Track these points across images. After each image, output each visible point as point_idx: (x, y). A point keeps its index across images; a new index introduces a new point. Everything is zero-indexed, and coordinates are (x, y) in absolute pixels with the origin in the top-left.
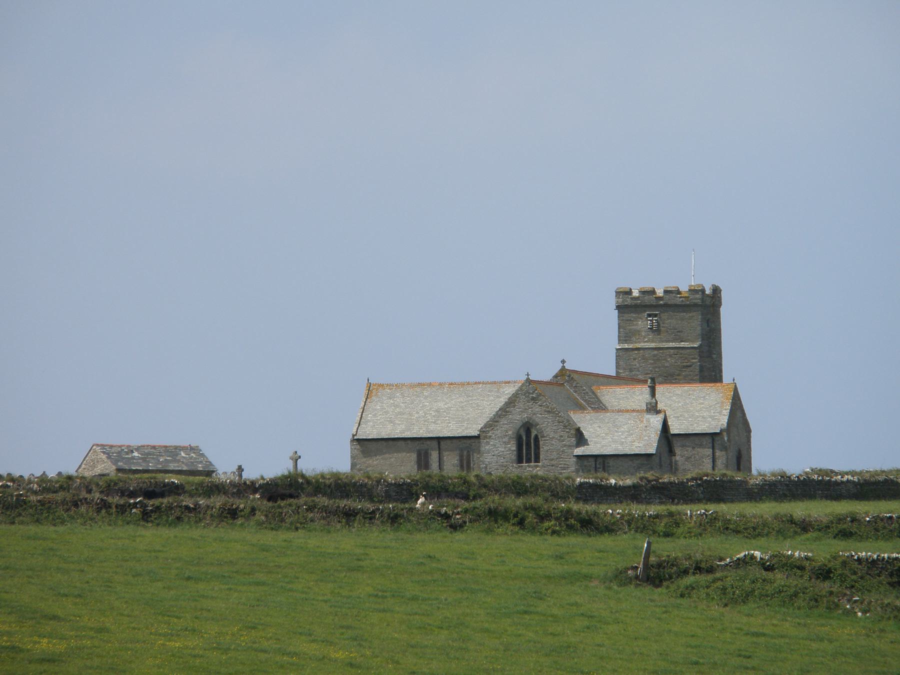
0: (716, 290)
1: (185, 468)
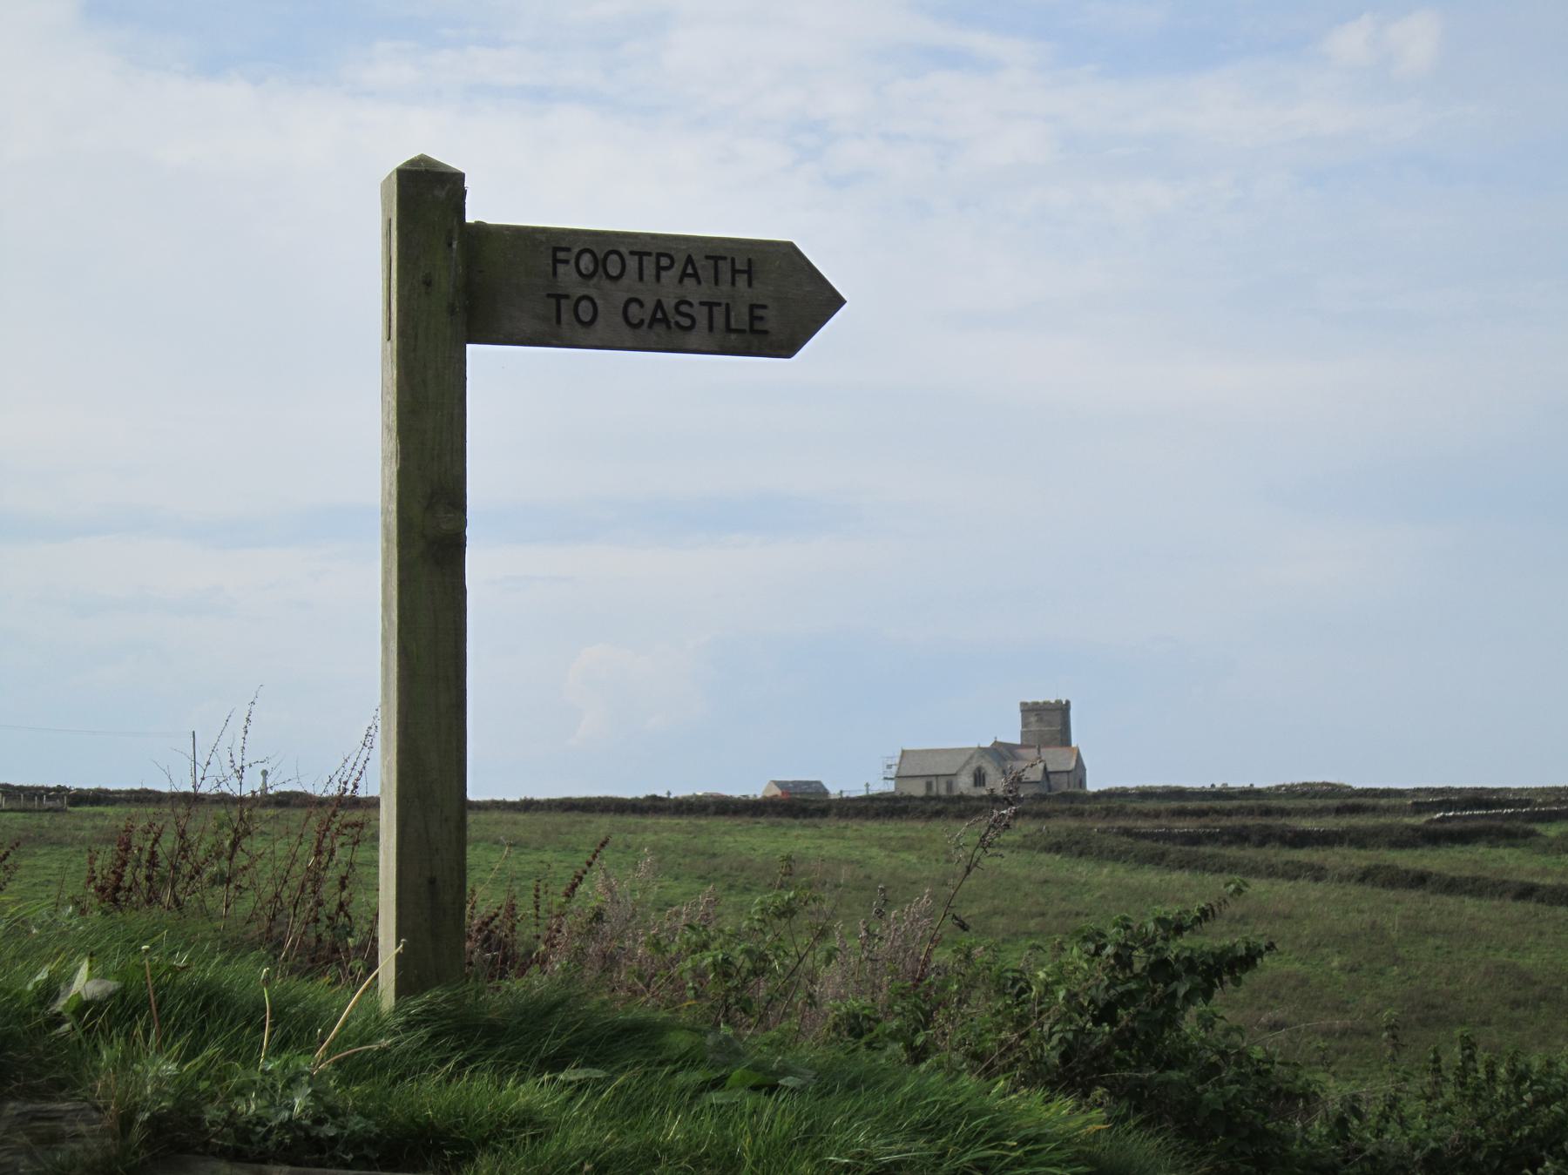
0: (1068, 703)
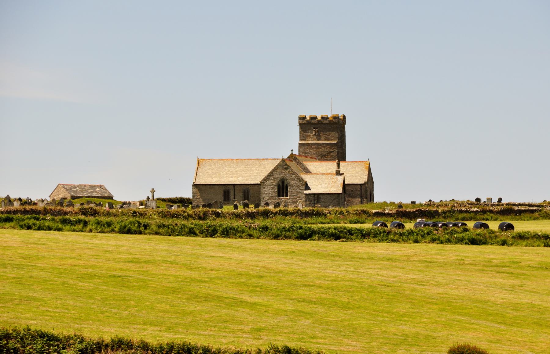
1: (100, 195)
